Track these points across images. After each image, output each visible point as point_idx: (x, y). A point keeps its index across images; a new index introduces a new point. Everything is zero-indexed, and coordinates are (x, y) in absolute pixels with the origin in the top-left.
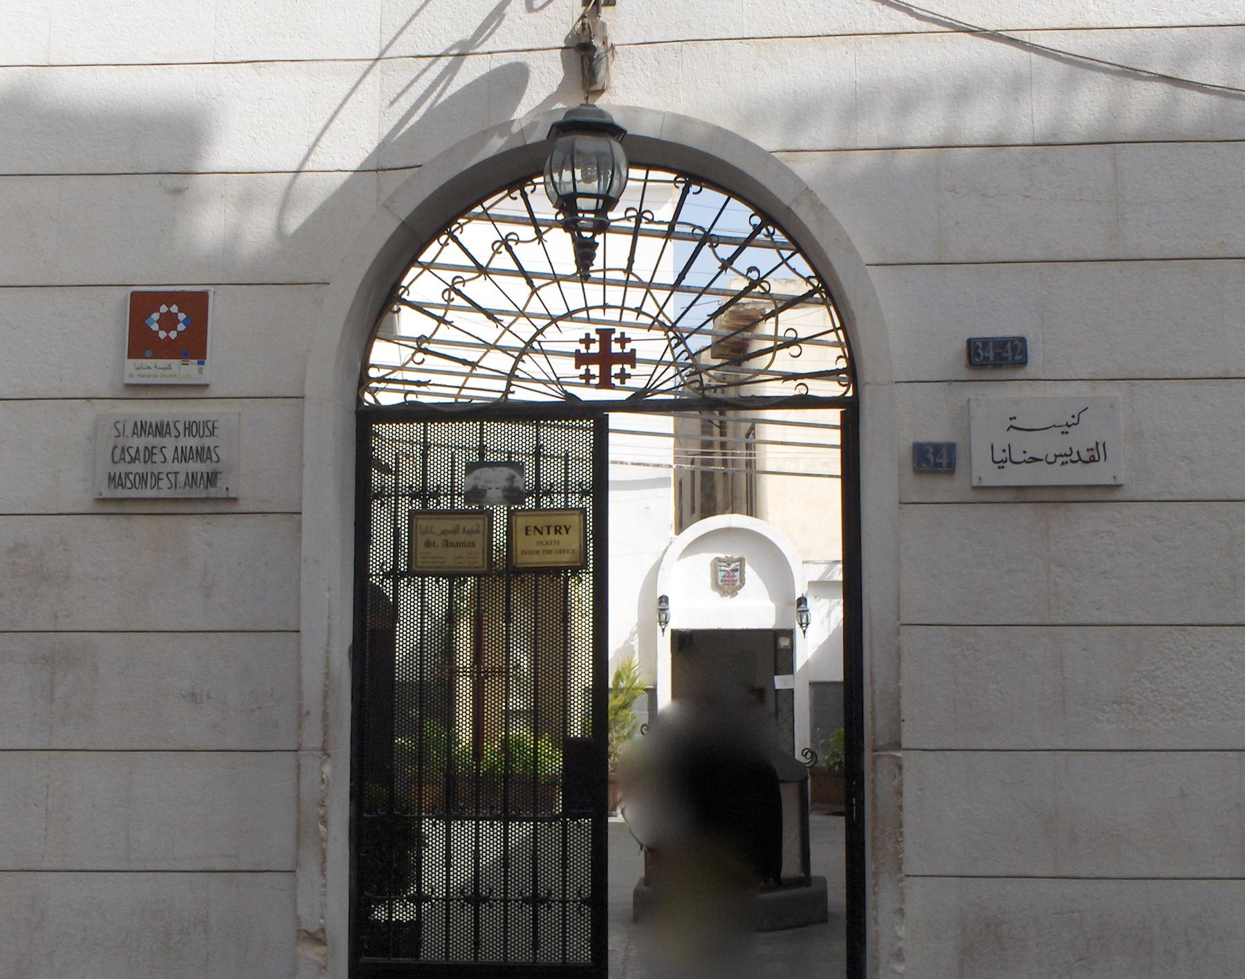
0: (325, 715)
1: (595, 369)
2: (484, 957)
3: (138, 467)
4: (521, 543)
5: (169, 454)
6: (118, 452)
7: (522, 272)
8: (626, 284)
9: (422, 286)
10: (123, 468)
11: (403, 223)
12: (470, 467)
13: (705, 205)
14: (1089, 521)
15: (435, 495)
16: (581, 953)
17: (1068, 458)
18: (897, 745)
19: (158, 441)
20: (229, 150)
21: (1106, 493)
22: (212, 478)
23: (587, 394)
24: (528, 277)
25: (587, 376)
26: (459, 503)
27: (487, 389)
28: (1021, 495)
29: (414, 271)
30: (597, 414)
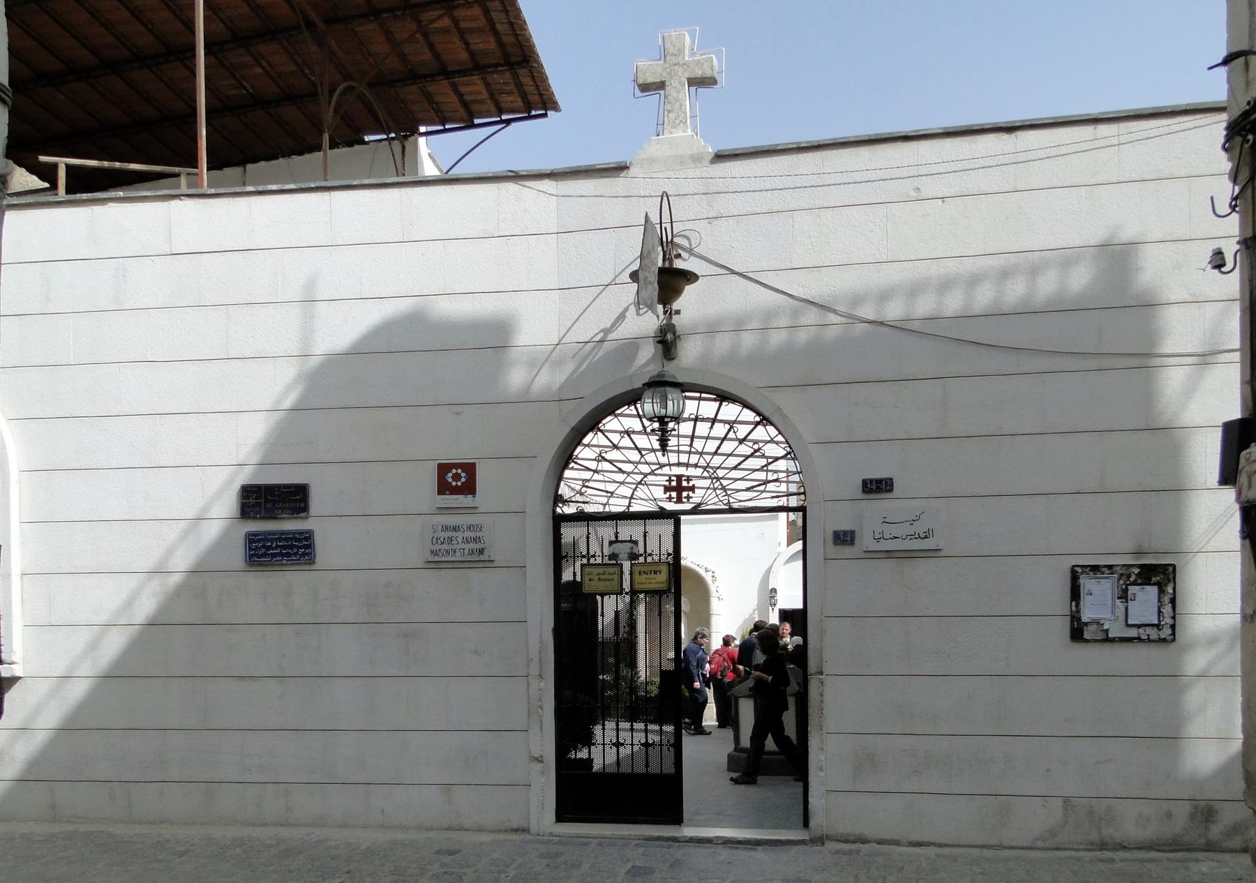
0: (540, 660)
1: (674, 494)
3: (445, 547)
4: (637, 578)
5: (460, 540)
7: (637, 448)
8: (690, 453)
9: (582, 453)
10: (437, 547)
12: (611, 543)
13: (730, 411)
14: (922, 568)
15: (594, 556)
16: (669, 769)
17: (912, 536)
18: (821, 673)
19: (455, 534)
21: (933, 553)
22: (481, 551)
23: (670, 506)
24: (639, 450)
25: (670, 498)
26: (606, 560)
27: (617, 506)
28: (888, 554)
29: (579, 448)
30: (675, 517)
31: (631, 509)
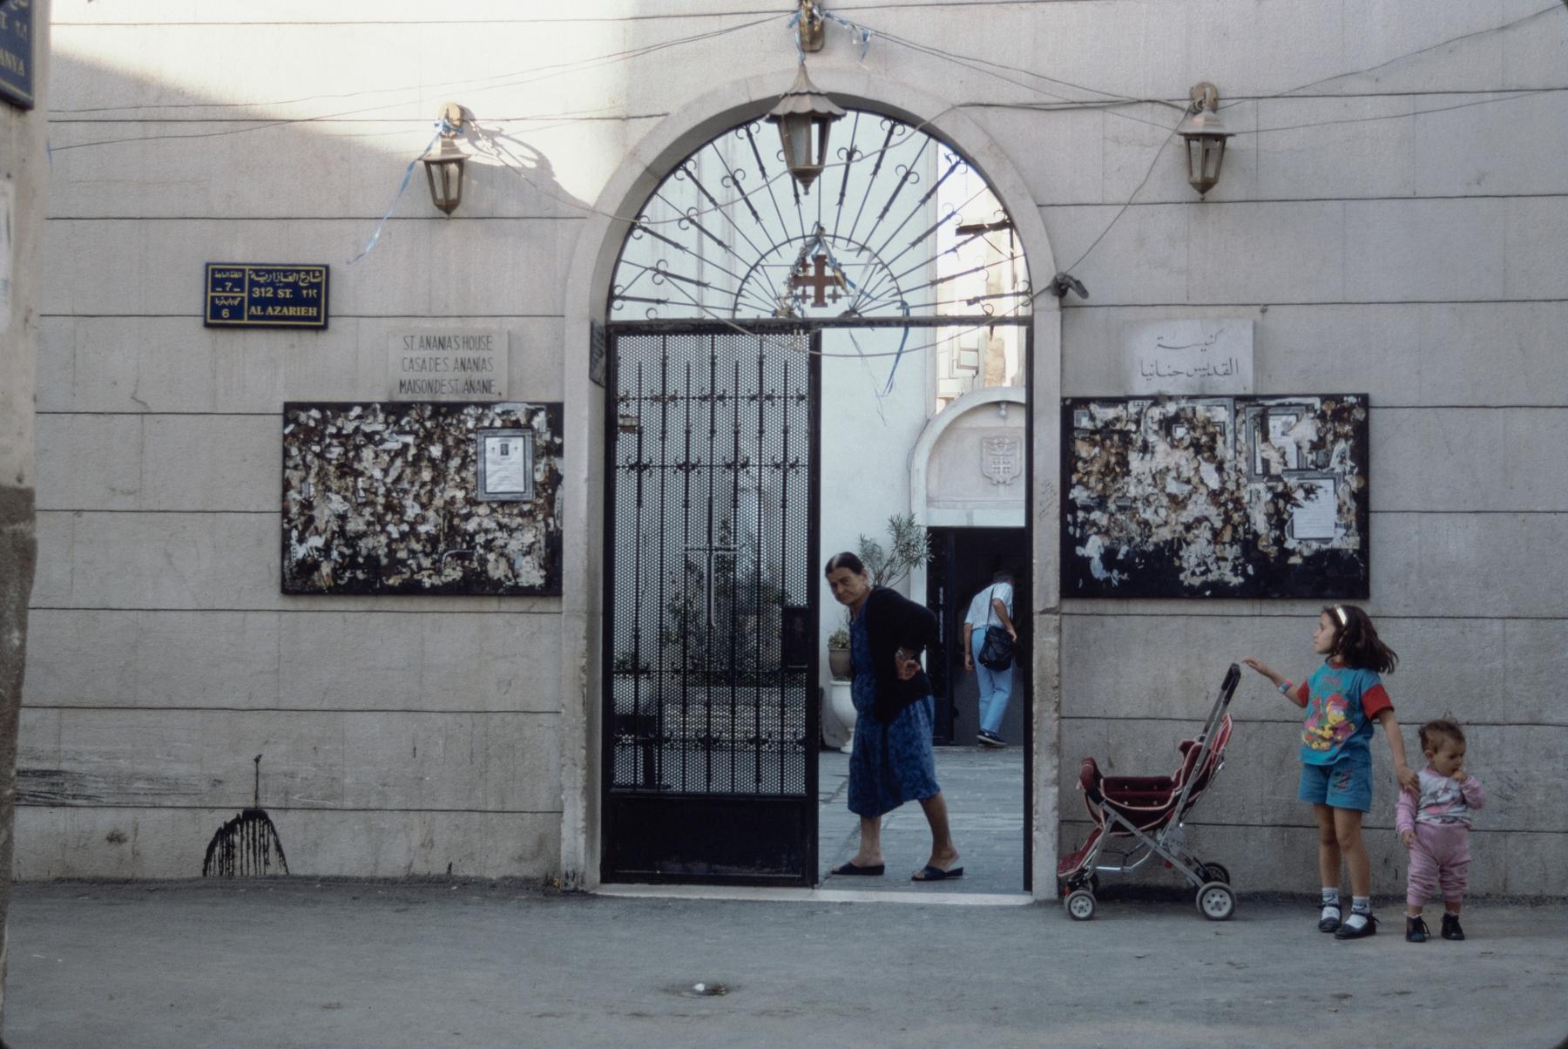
2: (715, 787)
5: (451, 363)
6: (407, 362)
11: (648, 169)
19: (441, 354)
20: (1324, 634)
30: (812, 329)
31: (739, 315)
